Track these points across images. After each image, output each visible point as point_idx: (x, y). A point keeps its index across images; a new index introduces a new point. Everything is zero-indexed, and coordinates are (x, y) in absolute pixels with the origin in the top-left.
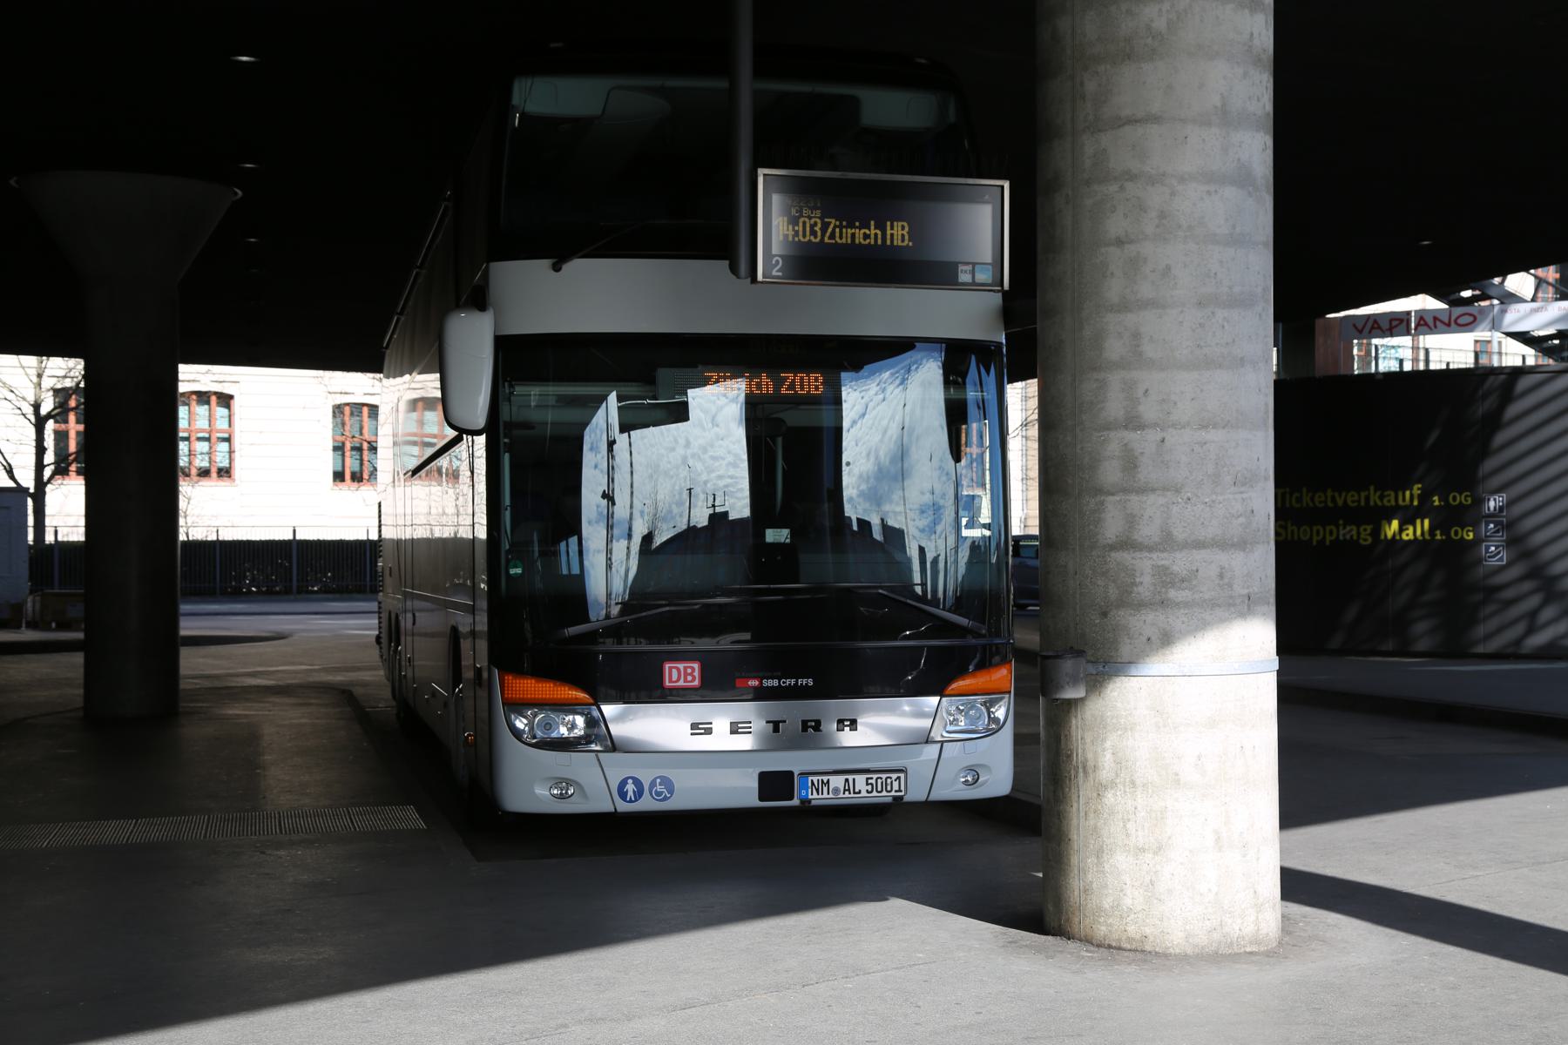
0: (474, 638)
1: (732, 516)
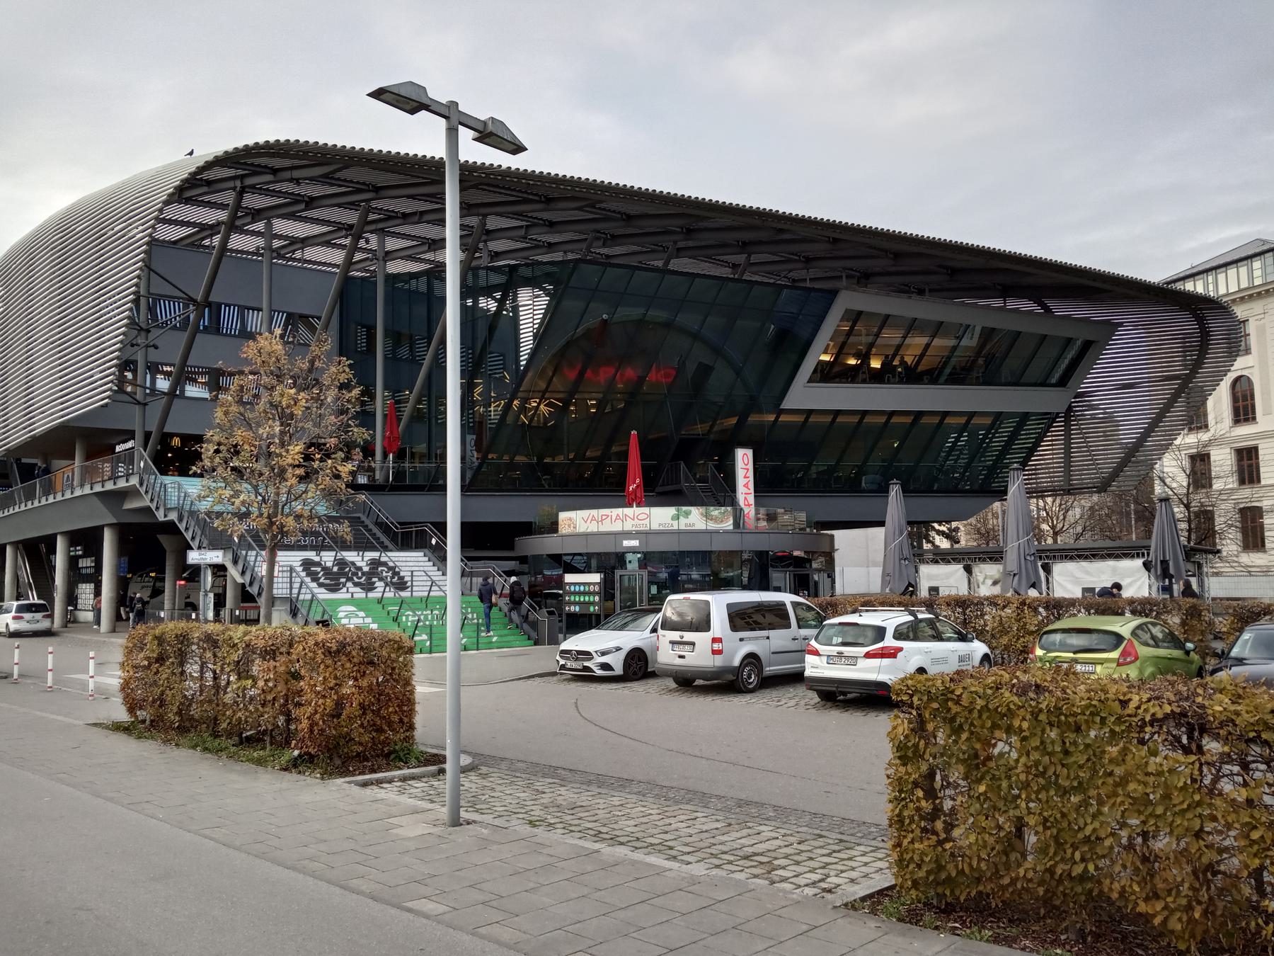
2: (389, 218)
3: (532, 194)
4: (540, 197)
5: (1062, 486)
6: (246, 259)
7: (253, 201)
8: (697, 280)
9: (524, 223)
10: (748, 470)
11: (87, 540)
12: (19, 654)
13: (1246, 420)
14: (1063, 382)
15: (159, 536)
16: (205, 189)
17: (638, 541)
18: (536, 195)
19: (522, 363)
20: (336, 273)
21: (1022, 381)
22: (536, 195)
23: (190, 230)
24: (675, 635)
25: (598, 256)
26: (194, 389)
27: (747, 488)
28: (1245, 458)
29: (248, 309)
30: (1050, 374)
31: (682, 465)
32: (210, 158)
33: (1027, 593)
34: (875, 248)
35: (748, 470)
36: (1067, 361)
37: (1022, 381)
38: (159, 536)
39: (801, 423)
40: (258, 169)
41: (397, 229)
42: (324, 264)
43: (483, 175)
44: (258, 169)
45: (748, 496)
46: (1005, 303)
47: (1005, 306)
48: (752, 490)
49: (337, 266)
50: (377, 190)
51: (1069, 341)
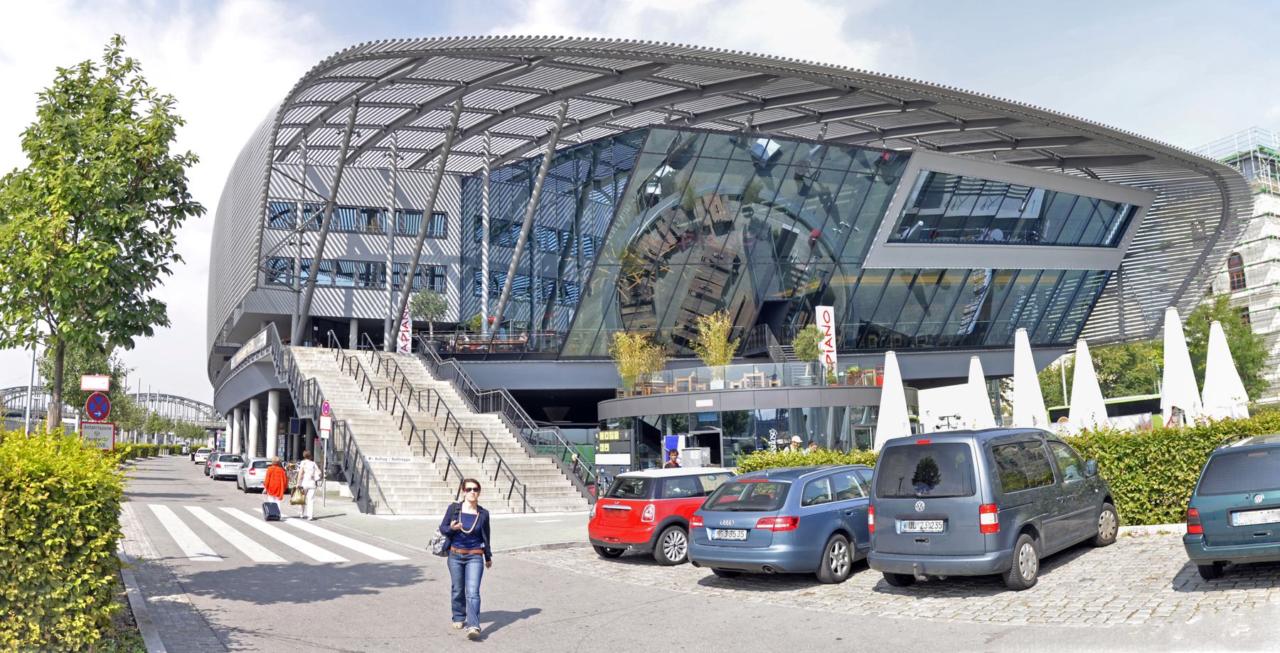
5: (1118, 336)
10: (829, 327)
11: (262, 400)
13: (1239, 287)
14: (1115, 243)
17: (711, 401)
19: (285, 276)
21: (1081, 242)
24: (808, 467)
26: (342, 280)
27: (829, 345)
29: (439, 214)
30: (1103, 237)
31: (767, 325)
32: (278, 109)
33: (878, 569)
35: (829, 327)
36: (1117, 224)
37: (1081, 242)
39: (882, 285)
45: (830, 354)
48: (834, 348)
51: (1117, 207)
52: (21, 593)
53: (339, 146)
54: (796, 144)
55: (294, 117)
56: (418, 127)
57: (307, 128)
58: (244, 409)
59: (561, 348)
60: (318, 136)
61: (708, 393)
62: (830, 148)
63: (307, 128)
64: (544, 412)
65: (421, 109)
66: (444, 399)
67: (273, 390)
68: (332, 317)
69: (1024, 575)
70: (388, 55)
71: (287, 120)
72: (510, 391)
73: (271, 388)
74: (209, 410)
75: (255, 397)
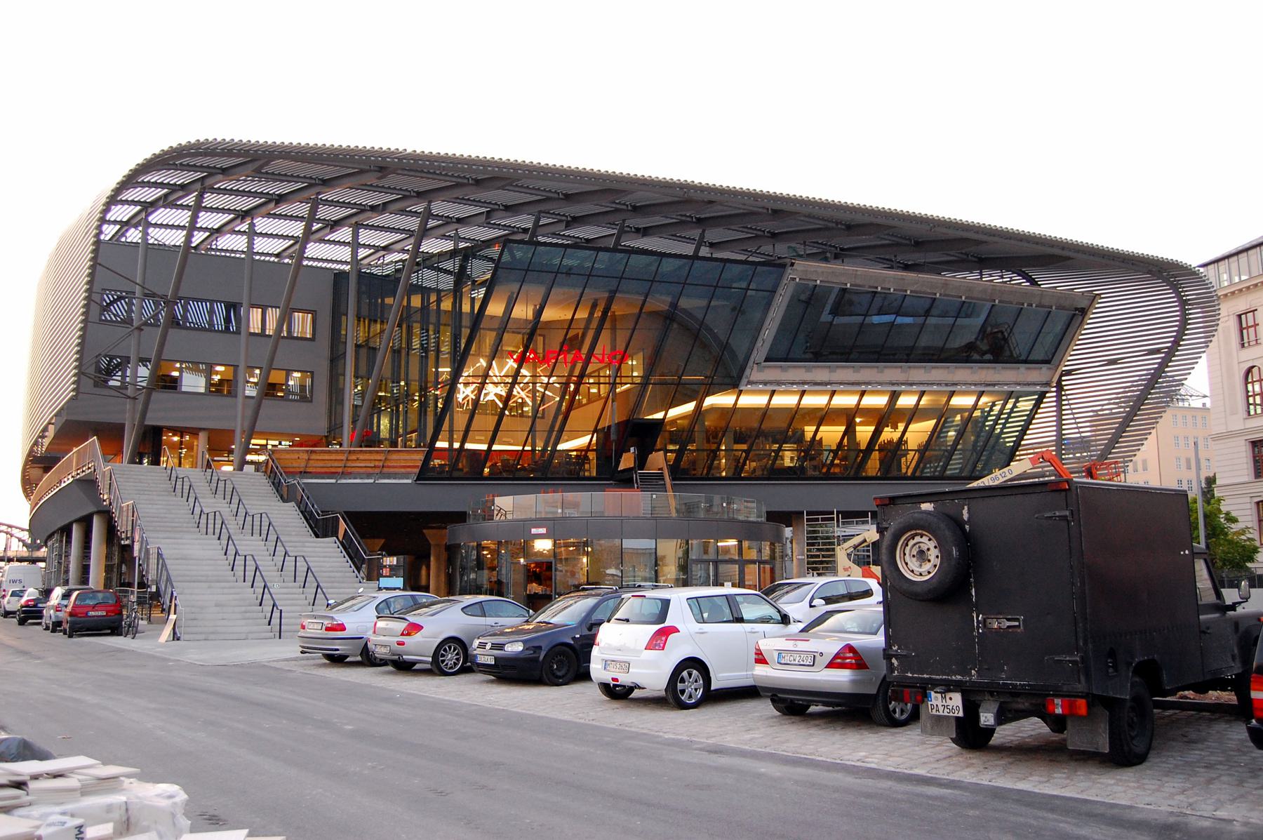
0: (703, 321)
1: (961, 714)
2: (362, 211)
3: (619, 203)
4: (559, 194)
6: (225, 256)
7: (325, 212)
8: (664, 260)
9: (484, 210)
11: (86, 522)
12: (518, 451)
15: (695, 402)
16: (181, 193)
18: (624, 204)
20: (291, 265)
22: (624, 204)
23: (481, 253)
25: (578, 240)
28: (114, 583)
34: (818, 219)
38: (695, 402)
40: (214, 171)
41: (370, 222)
42: (322, 260)
43: (396, 160)
44: (214, 171)
46: (981, 275)
47: (981, 278)
49: (346, 263)
50: (327, 183)
52: (182, 437)
53: (184, 226)
54: (659, 258)
55: (132, 194)
56: (280, 215)
57: (148, 207)
58: (66, 531)
59: (945, 468)
60: (159, 216)
61: (1217, 585)
62: (696, 261)
63: (148, 207)
64: (379, 537)
65: (280, 199)
66: (274, 524)
67: (98, 512)
68: (309, 210)
69: (897, 715)
70: (238, 155)
71: (124, 196)
72: (345, 512)
73: (95, 510)
74: (25, 536)
75: (78, 521)
